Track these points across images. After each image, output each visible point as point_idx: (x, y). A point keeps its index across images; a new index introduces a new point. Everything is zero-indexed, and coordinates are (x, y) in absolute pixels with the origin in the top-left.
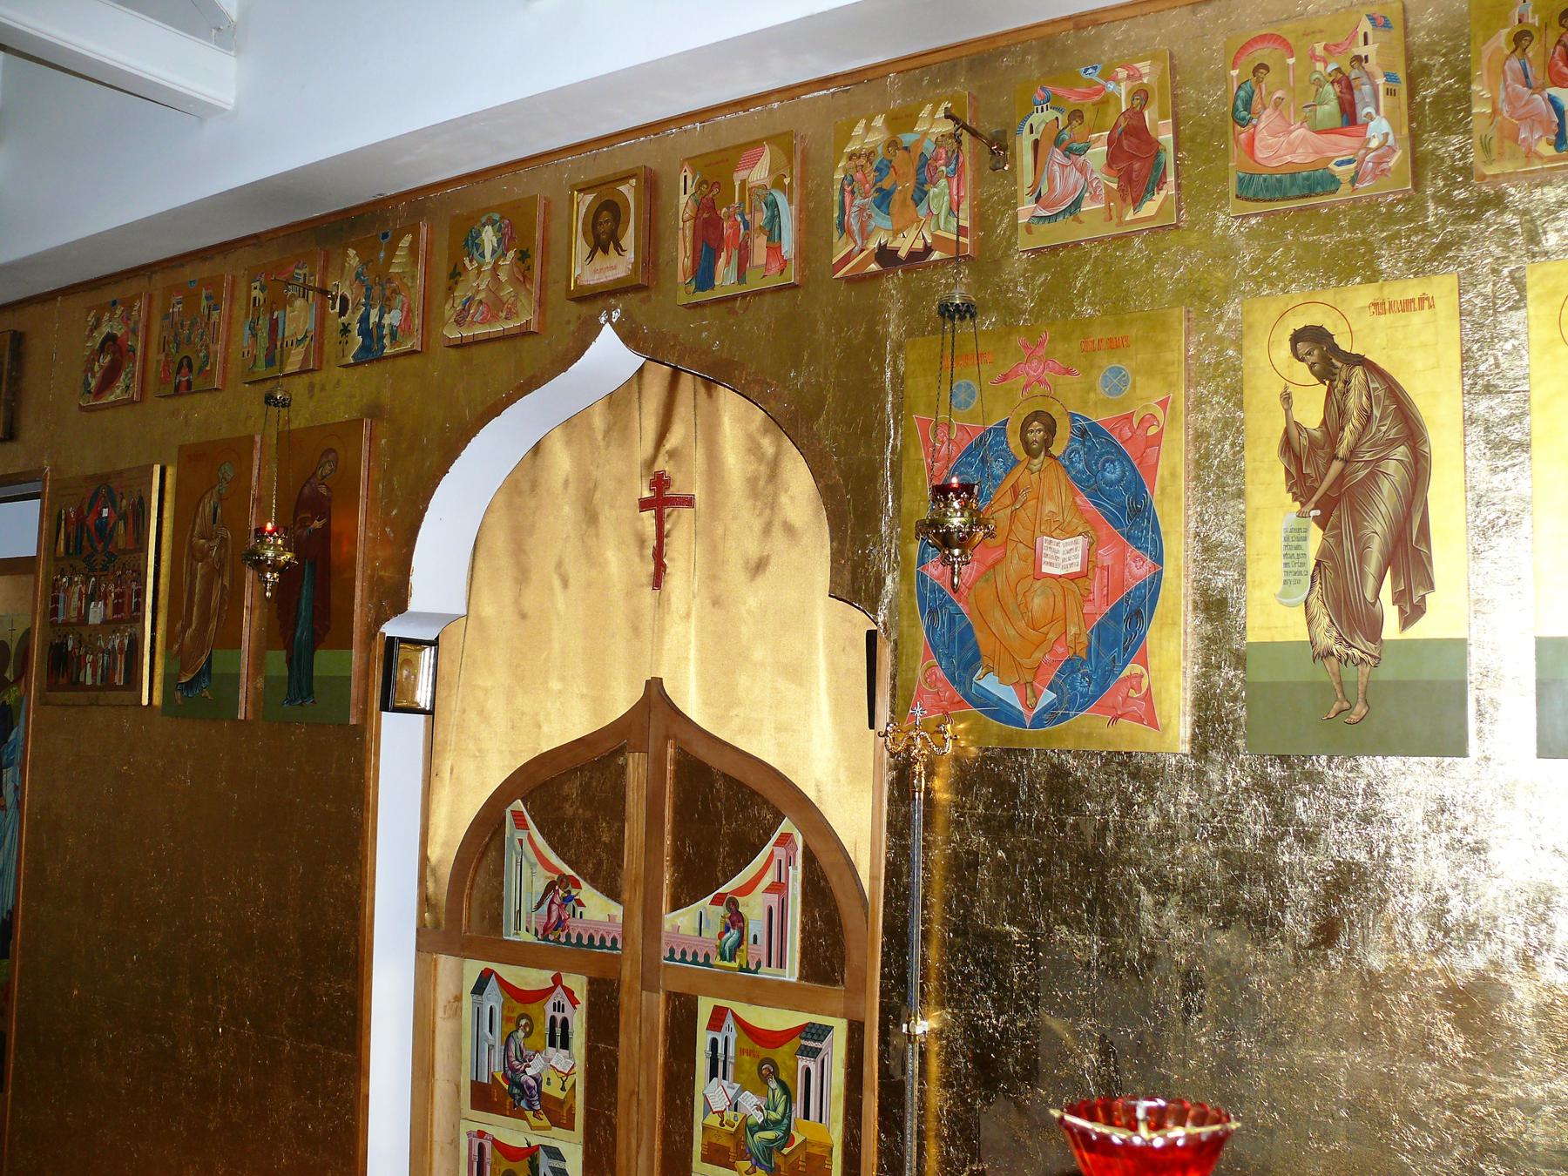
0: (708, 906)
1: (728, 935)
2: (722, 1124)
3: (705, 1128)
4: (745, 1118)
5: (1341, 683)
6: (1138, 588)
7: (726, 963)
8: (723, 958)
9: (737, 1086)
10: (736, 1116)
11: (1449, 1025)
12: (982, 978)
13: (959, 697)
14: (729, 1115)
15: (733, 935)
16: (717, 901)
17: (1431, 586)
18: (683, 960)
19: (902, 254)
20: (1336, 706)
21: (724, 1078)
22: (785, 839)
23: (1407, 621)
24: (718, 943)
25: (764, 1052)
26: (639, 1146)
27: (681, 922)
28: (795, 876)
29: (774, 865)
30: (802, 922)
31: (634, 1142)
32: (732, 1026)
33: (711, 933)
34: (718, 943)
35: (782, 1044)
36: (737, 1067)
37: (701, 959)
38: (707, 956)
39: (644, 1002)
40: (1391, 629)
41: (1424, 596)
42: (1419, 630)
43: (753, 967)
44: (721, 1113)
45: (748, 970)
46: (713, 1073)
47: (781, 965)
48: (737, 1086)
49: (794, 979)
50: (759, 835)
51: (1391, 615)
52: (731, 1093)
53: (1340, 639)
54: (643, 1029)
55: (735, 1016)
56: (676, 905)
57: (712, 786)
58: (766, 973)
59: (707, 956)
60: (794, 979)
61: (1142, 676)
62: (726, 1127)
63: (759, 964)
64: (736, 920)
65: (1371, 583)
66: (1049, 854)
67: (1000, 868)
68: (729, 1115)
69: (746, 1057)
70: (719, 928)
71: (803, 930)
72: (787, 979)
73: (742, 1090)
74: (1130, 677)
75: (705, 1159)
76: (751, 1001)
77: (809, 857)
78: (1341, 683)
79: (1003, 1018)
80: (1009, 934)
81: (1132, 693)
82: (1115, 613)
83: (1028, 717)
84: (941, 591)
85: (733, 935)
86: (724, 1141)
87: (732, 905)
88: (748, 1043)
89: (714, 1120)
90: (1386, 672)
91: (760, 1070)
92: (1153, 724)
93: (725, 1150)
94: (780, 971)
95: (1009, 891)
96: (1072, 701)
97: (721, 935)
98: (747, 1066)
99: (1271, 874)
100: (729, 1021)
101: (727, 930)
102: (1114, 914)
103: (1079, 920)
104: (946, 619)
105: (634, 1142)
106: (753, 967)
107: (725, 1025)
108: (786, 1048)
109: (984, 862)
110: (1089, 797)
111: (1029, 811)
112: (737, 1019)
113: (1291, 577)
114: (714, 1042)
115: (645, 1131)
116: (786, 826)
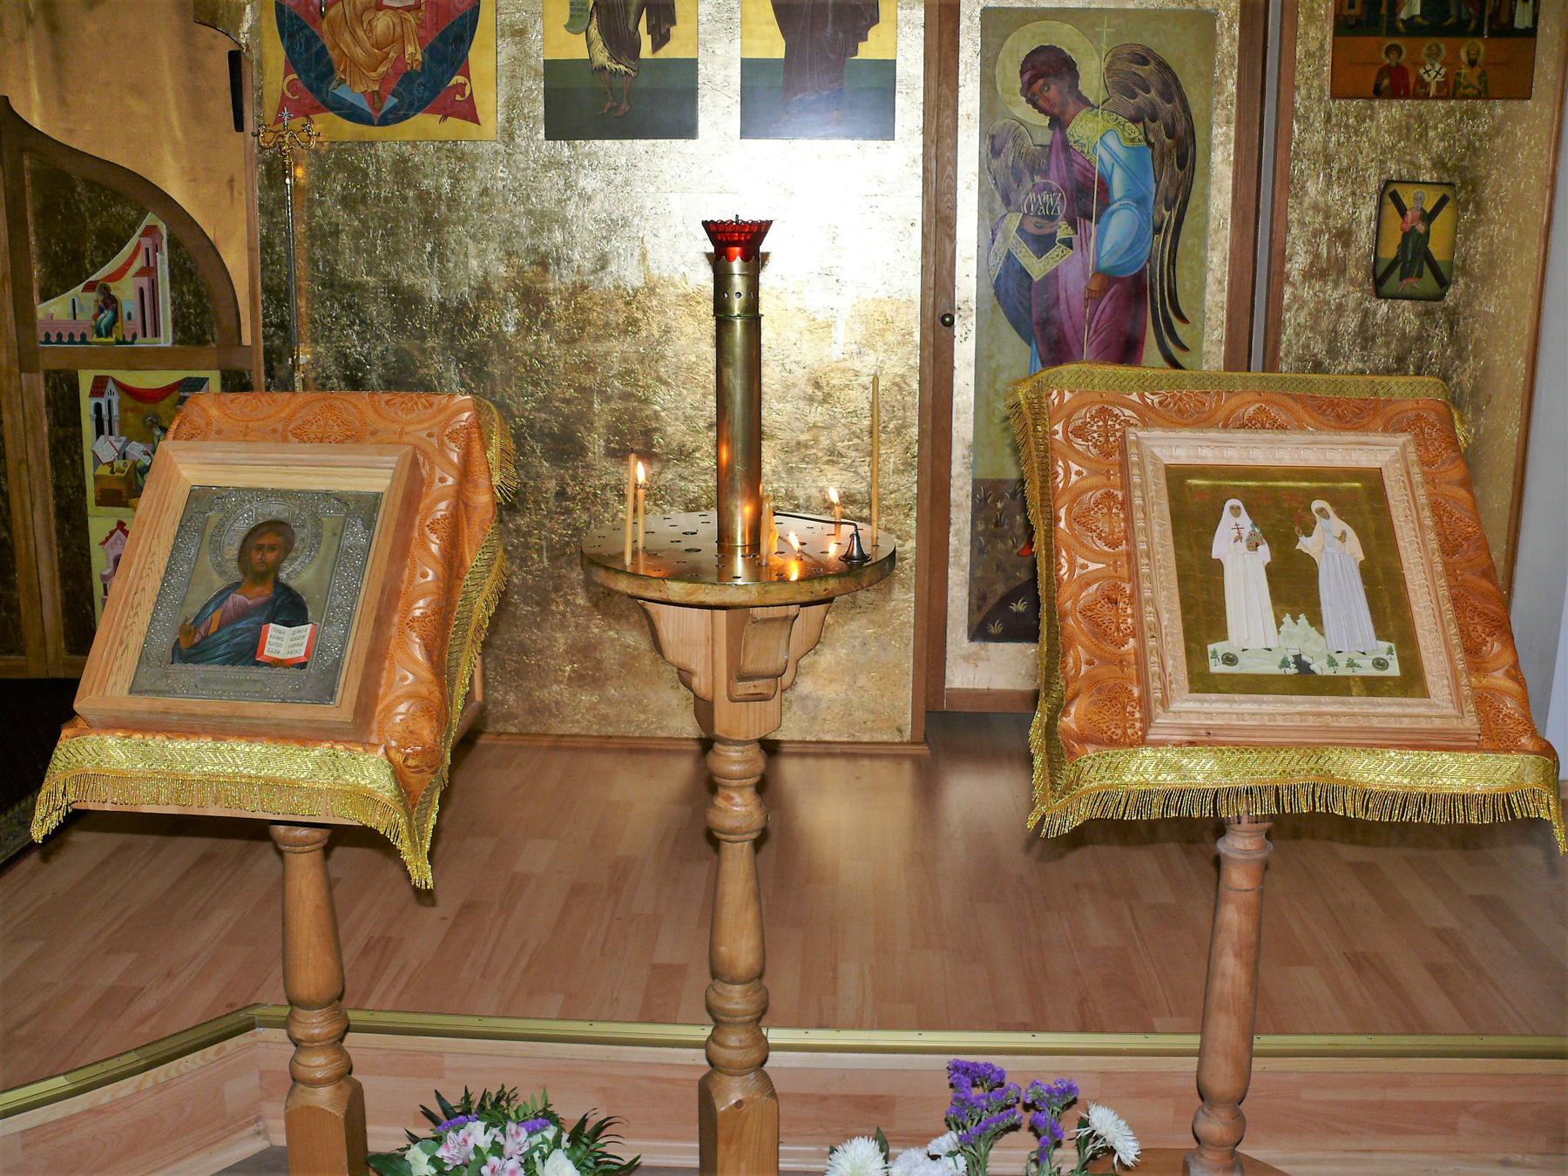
0: (80, 294)
1: (103, 315)
2: (112, 472)
3: (97, 478)
4: (135, 463)
5: (611, 89)
6: (461, 18)
7: (103, 339)
8: (99, 335)
9: (124, 438)
10: (125, 463)
11: (467, 289)
12: (347, 316)
13: (318, 103)
14: (119, 464)
15: (108, 314)
16: (90, 287)
17: (674, 23)
18: (60, 341)
19: (1306, 544)
20: (608, 105)
21: (111, 434)
22: (151, 231)
23: (656, 47)
24: (93, 323)
25: (146, 407)
26: (33, 504)
27: (54, 310)
28: (162, 260)
29: (142, 253)
30: (172, 297)
31: (28, 502)
32: (114, 390)
33: (85, 316)
34: (93, 323)
35: (163, 398)
36: (123, 424)
37: (78, 339)
38: (83, 336)
39: (24, 383)
40: (646, 51)
41: (669, 30)
42: (666, 52)
43: (129, 339)
44: (111, 464)
45: (126, 343)
46: (99, 431)
47: (156, 333)
48: (124, 438)
49: (169, 344)
50: (124, 229)
51: (646, 42)
52: (118, 445)
53: (611, 58)
54: (25, 404)
55: (115, 381)
56: (46, 296)
57: (73, 190)
58: (141, 343)
59: (83, 336)
60: (169, 344)
61: (465, 84)
62: (117, 474)
63: (134, 336)
64: (109, 302)
65: (632, 17)
66: (395, 219)
67: (357, 235)
68: (119, 464)
69: (130, 414)
70: (93, 311)
71: (173, 303)
72: (162, 345)
73: (128, 441)
74: (458, 85)
75: (99, 503)
76: (131, 368)
77: (174, 244)
78: (611, 89)
79: (367, 346)
80: (367, 282)
81: (458, 98)
82: (443, 37)
83: (376, 117)
84: (297, 18)
85: (108, 314)
86: (116, 486)
87: (105, 290)
88: (131, 402)
89: (104, 471)
90: (644, 82)
91: (144, 422)
92: (475, 120)
93: (119, 492)
94: (156, 339)
95: (366, 251)
96: (411, 105)
97: (95, 317)
98: (131, 420)
99: (564, 223)
100: (111, 386)
101: (101, 311)
102: (448, 261)
103: (421, 267)
104: (303, 41)
105: (28, 502)
106: (129, 339)
107: (107, 391)
108: (167, 401)
109: (343, 230)
110: (425, 176)
111: (378, 188)
112: (119, 385)
113: (577, 13)
114: (98, 407)
115: (38, 493)
116: (150, 219)
